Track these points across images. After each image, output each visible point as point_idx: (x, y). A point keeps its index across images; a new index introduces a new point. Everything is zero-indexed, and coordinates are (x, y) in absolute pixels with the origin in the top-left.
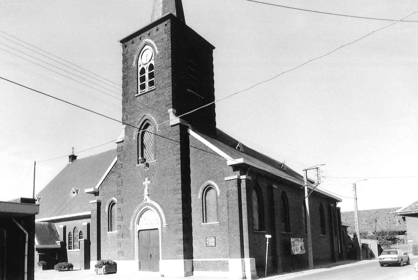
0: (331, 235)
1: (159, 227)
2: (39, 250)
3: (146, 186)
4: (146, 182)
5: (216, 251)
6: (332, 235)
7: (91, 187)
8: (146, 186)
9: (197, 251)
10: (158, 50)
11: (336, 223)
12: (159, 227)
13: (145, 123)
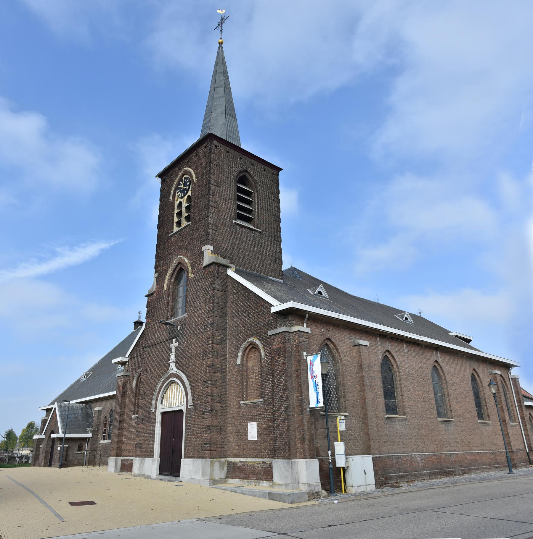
0: (503, 421)
1: (184, 408)
2: (64, 433)
3: (173, 350)
4: (174, 344)
5: (258, 446)
6: (504, 421)
7: (114, 390)
8: (173, 350)
9: (234, 445)
10: (196, 178)
11: (512, 399)
12: (184, 408)
13: (178, 268)
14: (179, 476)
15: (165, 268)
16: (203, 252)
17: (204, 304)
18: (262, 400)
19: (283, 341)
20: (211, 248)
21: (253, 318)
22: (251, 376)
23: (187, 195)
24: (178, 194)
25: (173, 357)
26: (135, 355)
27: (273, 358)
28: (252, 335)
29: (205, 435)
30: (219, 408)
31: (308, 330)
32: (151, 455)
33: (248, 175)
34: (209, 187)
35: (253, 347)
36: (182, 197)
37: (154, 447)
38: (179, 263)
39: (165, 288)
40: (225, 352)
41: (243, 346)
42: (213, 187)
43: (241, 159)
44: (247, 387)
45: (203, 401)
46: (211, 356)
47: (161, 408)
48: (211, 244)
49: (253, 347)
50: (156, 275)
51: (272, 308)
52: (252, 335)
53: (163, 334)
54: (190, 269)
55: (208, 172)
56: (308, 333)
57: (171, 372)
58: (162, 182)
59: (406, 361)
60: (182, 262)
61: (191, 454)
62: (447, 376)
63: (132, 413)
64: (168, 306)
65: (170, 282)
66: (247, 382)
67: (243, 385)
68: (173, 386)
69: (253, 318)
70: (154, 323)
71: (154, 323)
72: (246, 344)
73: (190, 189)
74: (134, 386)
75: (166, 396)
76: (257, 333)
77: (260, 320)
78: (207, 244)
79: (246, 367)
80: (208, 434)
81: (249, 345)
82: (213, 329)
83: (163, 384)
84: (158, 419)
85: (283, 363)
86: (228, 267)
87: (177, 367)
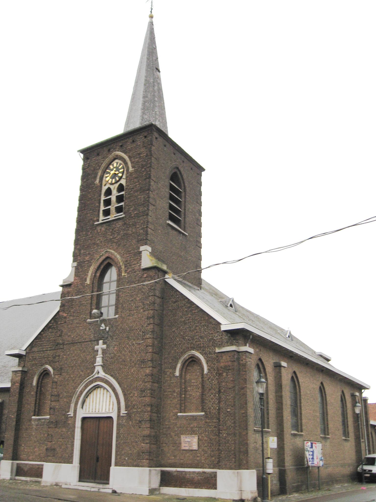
1: (115, 416)
3: (100, 352)
5: (198, 457)
8: (100, 352)
12: (115, 416)
13: (106, 263)
14: (108, 484)
15: (87, 258)
16: (140, 252)
17: (143, 308)
18: (203, 413)
19: (233, 360)
20: (149, 249)
21: (195, 331)
22: (189, 388)
23: (119, 183)
24: (107, 179)
25: (99, 360)
26: (35, 349)
27: (220, 374)
28: (194, 348)
29: (142, 444)
30: (156, 418)
31: (251, 350)
32: (69, 460)
33: (178, 172)
34: (149, 182)
35: (193, 361)
36: (112, 184)
37: (73, 453)
38: (108, 258)
39: (88, 282)
40: (161, 361)
41: (182, 359)
42: (152, 183)
43: (174, 154)
44: (185, 400)
45: (139, 410)
46: (151, 365)
47: (81, 414)
48: (150, 245)
49: (193, 361)
50: (75, 264)
51: (221, 326)
52: (193, 348)
53: (84, 333)
54: (123, 267)
55: (149, 165)
56: (251, 353)
57: (97, 376)
58: (84, 160)
59: (309, 384)
60: (113, 257)
61: (125, 463)
62: (327, 397)
63: (32, 414)
64: (91, 303)
65: (95, 276)
66: (185, 394)
67: (181, 397)
68: (99, 392)
69: (195, 331)
70: (72, 318)
71: (72, 318)
72: (186, 356)
73: (124, 177)
74: (35, 383)
75: (88, 400)
76: (200, 347)
77: (203, 335)
78: (146, 244)
79: (185, 379)
80: (147, 443)
81: (189, 358)
82: (153, 338)
83: (86, 387)
84: (78, 424)
85: (232, 381)
86: (165, 272)
87: (105, 371)
